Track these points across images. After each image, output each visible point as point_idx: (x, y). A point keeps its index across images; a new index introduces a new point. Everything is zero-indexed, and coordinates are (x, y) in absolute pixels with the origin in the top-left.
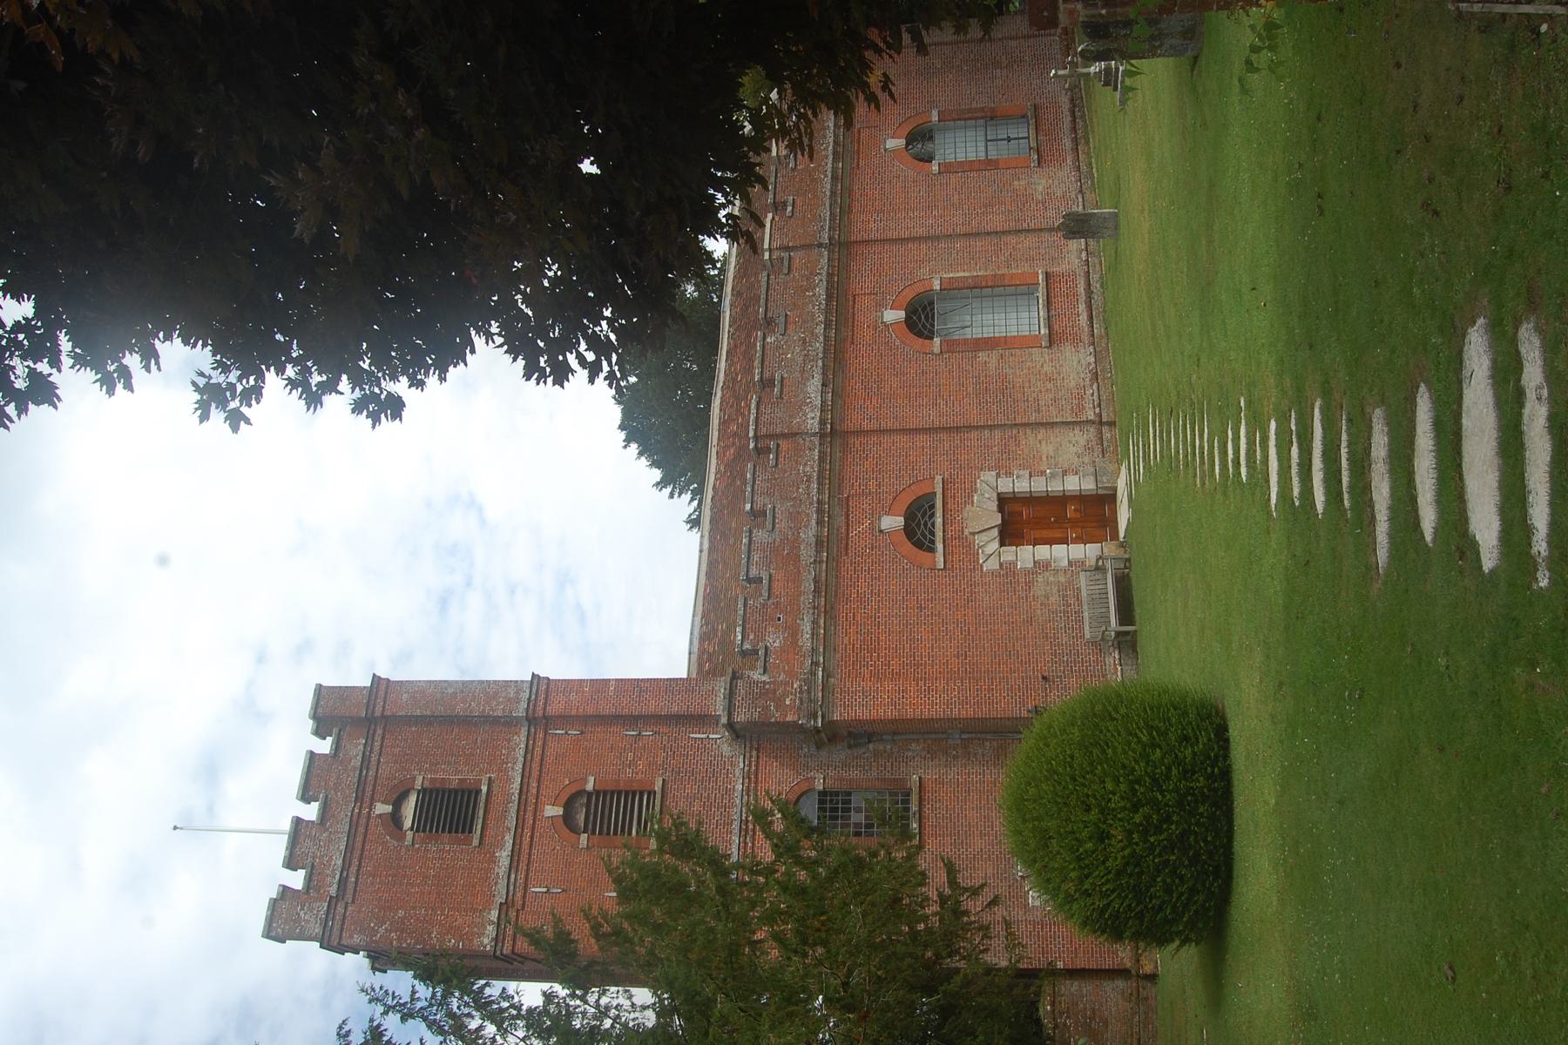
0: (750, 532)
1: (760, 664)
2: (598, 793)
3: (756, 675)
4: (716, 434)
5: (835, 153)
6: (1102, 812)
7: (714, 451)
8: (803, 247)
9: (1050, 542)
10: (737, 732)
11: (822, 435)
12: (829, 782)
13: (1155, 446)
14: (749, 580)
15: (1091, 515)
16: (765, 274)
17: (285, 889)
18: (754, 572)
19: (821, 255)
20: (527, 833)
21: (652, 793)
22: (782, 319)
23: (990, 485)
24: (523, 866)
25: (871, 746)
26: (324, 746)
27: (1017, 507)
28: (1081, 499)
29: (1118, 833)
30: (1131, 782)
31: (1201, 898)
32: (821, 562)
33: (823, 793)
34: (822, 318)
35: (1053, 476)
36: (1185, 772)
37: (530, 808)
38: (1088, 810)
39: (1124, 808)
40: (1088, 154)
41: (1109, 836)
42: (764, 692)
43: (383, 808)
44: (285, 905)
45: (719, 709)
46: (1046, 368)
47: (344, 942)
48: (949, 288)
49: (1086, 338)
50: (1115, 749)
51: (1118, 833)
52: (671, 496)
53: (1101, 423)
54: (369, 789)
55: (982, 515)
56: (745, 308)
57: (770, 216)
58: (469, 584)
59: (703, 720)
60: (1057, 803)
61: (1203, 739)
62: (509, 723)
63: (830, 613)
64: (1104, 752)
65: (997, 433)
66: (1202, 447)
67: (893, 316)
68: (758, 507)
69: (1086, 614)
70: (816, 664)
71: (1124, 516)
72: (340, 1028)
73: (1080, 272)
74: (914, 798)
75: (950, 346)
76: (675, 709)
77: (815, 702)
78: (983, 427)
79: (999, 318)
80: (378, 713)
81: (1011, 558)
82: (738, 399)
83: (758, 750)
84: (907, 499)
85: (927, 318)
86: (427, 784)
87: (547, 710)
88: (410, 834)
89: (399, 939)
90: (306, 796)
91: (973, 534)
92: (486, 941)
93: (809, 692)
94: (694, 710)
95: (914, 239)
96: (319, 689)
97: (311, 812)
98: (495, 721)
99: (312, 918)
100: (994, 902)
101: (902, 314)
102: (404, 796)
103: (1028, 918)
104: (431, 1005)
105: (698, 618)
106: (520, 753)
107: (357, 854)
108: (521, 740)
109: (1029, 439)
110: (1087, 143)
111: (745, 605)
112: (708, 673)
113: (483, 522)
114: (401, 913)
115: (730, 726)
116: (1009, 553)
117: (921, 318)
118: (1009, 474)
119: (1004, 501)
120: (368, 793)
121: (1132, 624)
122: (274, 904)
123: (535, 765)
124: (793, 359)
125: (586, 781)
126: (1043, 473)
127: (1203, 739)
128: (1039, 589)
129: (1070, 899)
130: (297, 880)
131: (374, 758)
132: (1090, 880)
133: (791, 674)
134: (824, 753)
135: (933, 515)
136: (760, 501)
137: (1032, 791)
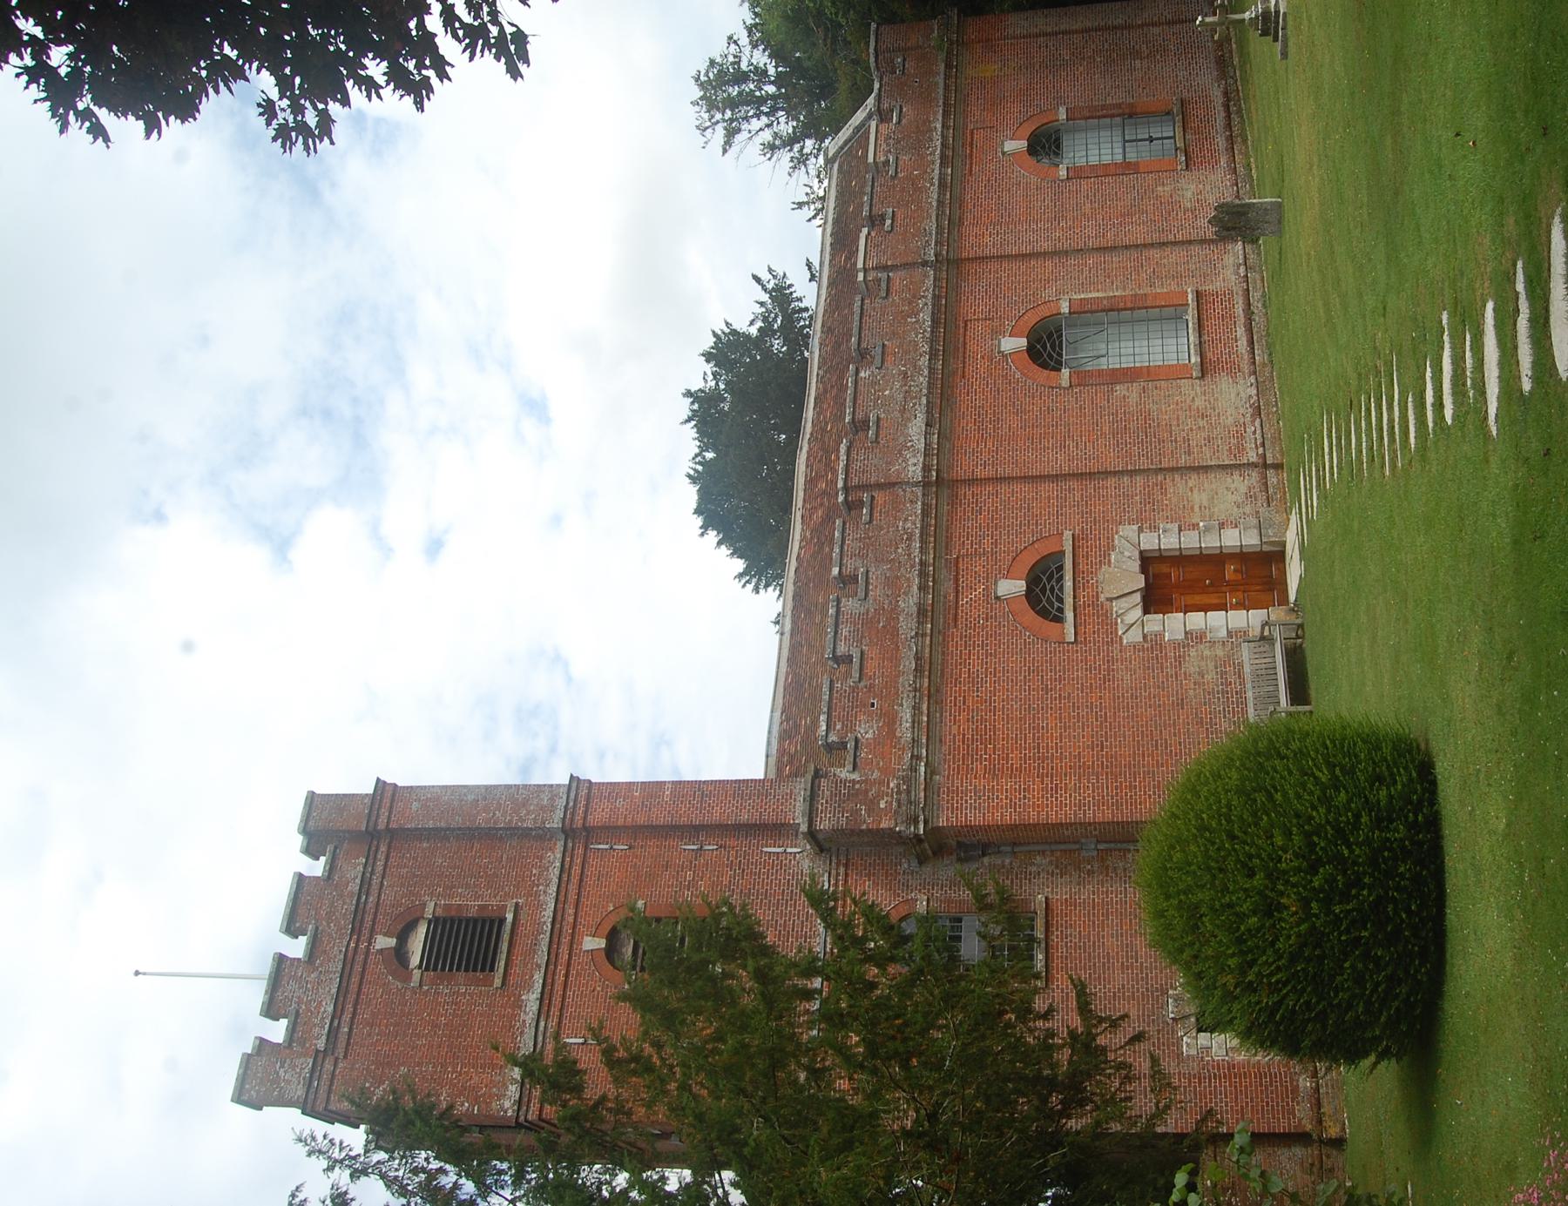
0: (838, 601)
3: (844, 773)
4: (801, 494)
5: (943, 156)
6: (1269, 876)
7: (799, 515)
8: (905, 266)
9: (1205, 609)
10: (820, 843)
11: (926, 484)
13: (1331, 459)
14: (836, 659)
15: (1256, 574)
16: (858, 298)
17: (262, 1043)
18: (842, 649)
19: (926, 276)
20: (561, 970)
22: (879, 350)
24: (555, 1011)
25: (986, 860)
26: (317, 868)
27: (1164, 569)
28: (1242, 557)
30: (1308, 835)
31: (1403, 990)
34: (926, 348)
35: (1207, 529)
36: (1379, 820)
37: (565, 940)
38: (1251, 875)
39: (1298, 870)
40: (1247, 156)
41: (1281, 908)
42: (854, 793)
43: (384, 942)
46: (1197, 403)
47: (332, 1107)
48: (1081, 311)
49: (1246, 368)
52: (756, 590)
53: (1265, 466)
54: (368, 918)
55: (1121, 576)
56: (838, 345)
57: (865, 231)
58: (553, 750)
59: (778, 830)
60: (1209, 869)
61: (1402, 779)
62: (542, 836)
63: (934, 696)
64: (1271, 798)
65: (1139, 479)
66: (1391, 421)
67: (1013, 344)
68: (848, 571)
69: (1250, 694)
70: (919, 758)
71: (1294, 572)
72: (293, 1196)
73: (1238, 290)
74: (1040, 923)
75: (1082, 378)
76: (744, 817)
77: (917, 803)
78: (1122, 473)
79: (1141, 346)
80: (381, 826)
82: (827, 452)
83: (846, 866)
84: (1030, 559)
86: (439, 912)
87: (588, 822)
88: (417, 974)
90: (292, 927)
91: (1111, 600)
92: (507, 1104)
93: (908, 792)
94: (769, 817)
96: (312, 799)
97: (297, 948)
98: (525, 834)
99: (294, 1077)
100: (1138, 1038)
102: (410, 927)
105: (778, 714)
106: (554, 874)
107: (351, 997)
109: (1179, 487)
110: (1245, 141)
111: (831, 690)
113: (569, 679)
115: (812, 835)
116: (1154, 622)
117: (1045, 347)
119: (1148, 561)
121: (1307, 703)
122: (247, 1060)
123: (573, 888)
124: (891, 397)
126: (1195, 526)
127: (1402, 779)
128: (1191, 666)
129: (1229, 997)
130: (277, 1031)
131: (376, 881)
132: (1256, 969)
133: (885, 771)
134: (927, 869)
135: (1061, 578)
137: (1177, 856)
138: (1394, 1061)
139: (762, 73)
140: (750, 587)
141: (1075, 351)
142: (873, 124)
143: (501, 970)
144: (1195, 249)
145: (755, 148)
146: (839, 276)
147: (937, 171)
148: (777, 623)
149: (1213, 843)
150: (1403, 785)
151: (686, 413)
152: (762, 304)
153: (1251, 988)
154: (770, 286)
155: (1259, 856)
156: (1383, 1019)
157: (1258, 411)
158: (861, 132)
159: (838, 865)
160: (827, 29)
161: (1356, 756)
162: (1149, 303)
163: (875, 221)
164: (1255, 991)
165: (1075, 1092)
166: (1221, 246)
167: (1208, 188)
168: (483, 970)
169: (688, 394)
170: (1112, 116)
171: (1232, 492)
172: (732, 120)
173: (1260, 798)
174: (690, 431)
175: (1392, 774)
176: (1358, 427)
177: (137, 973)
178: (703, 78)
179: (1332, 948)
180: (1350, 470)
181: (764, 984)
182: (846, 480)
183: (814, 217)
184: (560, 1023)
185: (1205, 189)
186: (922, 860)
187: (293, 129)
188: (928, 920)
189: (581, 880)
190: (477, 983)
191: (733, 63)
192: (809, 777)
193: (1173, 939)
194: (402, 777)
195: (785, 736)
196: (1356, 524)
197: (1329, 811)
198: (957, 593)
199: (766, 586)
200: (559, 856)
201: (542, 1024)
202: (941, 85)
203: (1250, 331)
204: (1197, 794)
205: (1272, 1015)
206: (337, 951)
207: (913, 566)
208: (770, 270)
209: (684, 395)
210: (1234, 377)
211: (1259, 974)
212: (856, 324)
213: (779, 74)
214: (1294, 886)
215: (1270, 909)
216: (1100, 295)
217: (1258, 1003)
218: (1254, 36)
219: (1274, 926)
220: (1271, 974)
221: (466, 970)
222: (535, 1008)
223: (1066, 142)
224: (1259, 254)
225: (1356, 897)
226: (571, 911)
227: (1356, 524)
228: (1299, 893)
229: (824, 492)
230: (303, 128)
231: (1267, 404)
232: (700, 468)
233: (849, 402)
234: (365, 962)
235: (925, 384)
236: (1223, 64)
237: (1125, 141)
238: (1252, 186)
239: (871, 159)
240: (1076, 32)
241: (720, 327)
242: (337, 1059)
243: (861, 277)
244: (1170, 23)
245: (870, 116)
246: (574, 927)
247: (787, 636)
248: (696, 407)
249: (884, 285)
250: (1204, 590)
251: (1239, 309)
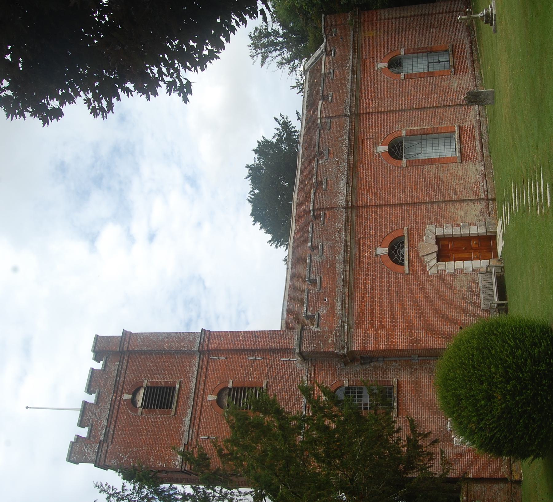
0: (311, 257)
1: (316, 322)
2: (234, 388)
3: (314, 328)
4: (295, 211)
5: (353, 70)
6: (489, 384)
7: (294, 219)
8: (337, 116)
9: (463, 260)
10: (304, 357)
11: (347, 208)
12: (351, 382)
13: (515, 202)
15: (484, 245)
16: (318, 130)
17: (78, 438)
18: (312, 277)
19: (346, 120)
20: (199, 408)
21: (261, 388)
22: (327, 152)
23: (431, 232)
24: (196, 425)
25: (372, 364)
26: (99, 366)
27: (446, 243)
28: (478, 238)
29: (498, 395)
30: (505, 368)
32: (346, 271)
33: (348, 388)
34: (346, 151)
37: (200, 396)
38: (482, 383)
39: (502, 382)
41: (494, 397)
42: (318, 337)
43: (127, 396)
44: (78, 445)
45: (295, 345)
47: (107, 464)
48: (411, 135)
49: (480, 158)
50: (496, 350)
51: (498, 395)
52: (276, 247)
53: (488, 199)
54: (120, 387)
55: (428, 246)
57: (321, 102)
59: (287, 351)
60: (465, 380)
61: (544, 344)
62: (190, 353)
63: (351, 296)
64: (490, 352)
65: (435, 206)
66: (540, 193)
67: (382, 149)
68: (315, 243)
69: (482, 296)
70: (344, 322)
73: (476, 125)
75: (411, 163)
76: (273, 346)
77: (344, 341)
78: (428, 203)
80: (125, 349)
81: (443, 268)
82: (306, 193)
83: (315, 366)
84: (390, 239)
85: (399, 150)
86: (149, 384)
87: (211, 348)
88: (140, 409)
89: (134, 462)
90: (89, 390)
91: (424, 256)
92: (177, 463)
93: (340, 336)
94: (283, 346)
95: (392, 111)
96: (97, 337)
98: (183, 352)
101: (386, 148)
102: (137, 390)
103: (455, 449)
104: (133, 493)
105: (286, 302)
106: (195, 369)
108: (196, 362)
109: (452, 209)
110: (479, 62)
111: (308, 293)
112: (291, 329)
114: (135, 449)
115: (301, 354)
116: (442, 265)
117: (396, 150)
118: (442, 226)
119: (439, 240)
120: (120, 389)
121: (506, 299)
122: (72, 444)
124: (332, 171)
125: (228, 382)
126: (458, 225)
127: (544, 344)
128: (457, 284)
129: (472, 433)
130: (84, 432)
131: (123, 372)
133: (331, 327)
134: (348, 368)
135: (403, 247)
136: (315, 241)
137: (451, 374)
138: (541, 458)
139: (276, 33)
140: (274, 246)
141: (408, 152)
142: (324, 57)
143: (174, 408)
144: (458, 108)
145: (274, 64)
146: (310, 120)
147: (350, 77)
148: (285, 260)
149: (466, 370)
150: (545, 347)
151: (247, 174)
152: (278, 129)
153: (482, 430)
154: (281, 122)
155: (485, 376)
156: (536, 443)
157: (485, 177)
158: (318, 60)
159: (311, 366)
160: (304, 14)
161: (525, 334)
162: (439, 131)
163: (325, 97)
164: (483, 430)
165: (410, 465)
166: (469, 107)
167: (463, 82)
168: (167, 408)
169: (248, 166)
170: (423, 52)
171: (474, 211)
172: (265, 53)
173: (486, 352)
174: (249, 182)
175: (540, 342)
176: (526, 192)
177: (27, 408)
178: (252, 35)
179: (515, 414)
180: (523, 208)
181: (283, 431)
182: (313, 206)
183: (300, 92)
184: (198, 430)
185: (462, 84)
186: (346, 364)
187: (98, 109)
188: (349, 390)
189: (206, 372)
191: (265, 29)
192: (299, 330)
193: (449, 408)
194: (134, 329)
195: (289, 311)
196: (525, 231)
197: (514, 358)
199: (280, 245)
200: (197, 361)
201: (191, 430)
202: (352, 40)
203: (481, 142)
204: (459, 350)
205: (491, 440)
206: (108, 400)
207: (341, 242)
208: (281, 115)
209: (246, 167)
210: (475, 162)
211: (485, 424)
212: (317, 141)
213: (284, 33)
214: (499, 388)
215: (489, 398)
216: (419, 128)
217: (485, 435)
218: (482, 23)
219: (491, 405)
220: (490, 424)
222: (188, 424)
223: (404, 63)
224: (485, 110)
225: (525, 393)
226: (203, 384)
227: (525, 231)
228: (501, 392)
229: (304, 210)
230: (101, 109)
231: (489, 174)
232: (253, 197)
233: (314, 173)
234: (119, 405)
235: (346, 166)
236: (469, 29)
237: (428, 63)
238: (482, 82)
239: (323, 72)
240: (408, 17)
241: (261, 139)
242: (108, 444)
243: (319, 121)
244: (447, 12)
245: (322, 53)
246: (204, 391)
247: (290, 270)
248: (251, 172)
249: (329, 125)
250: (463, 252)
251: (477, 134)
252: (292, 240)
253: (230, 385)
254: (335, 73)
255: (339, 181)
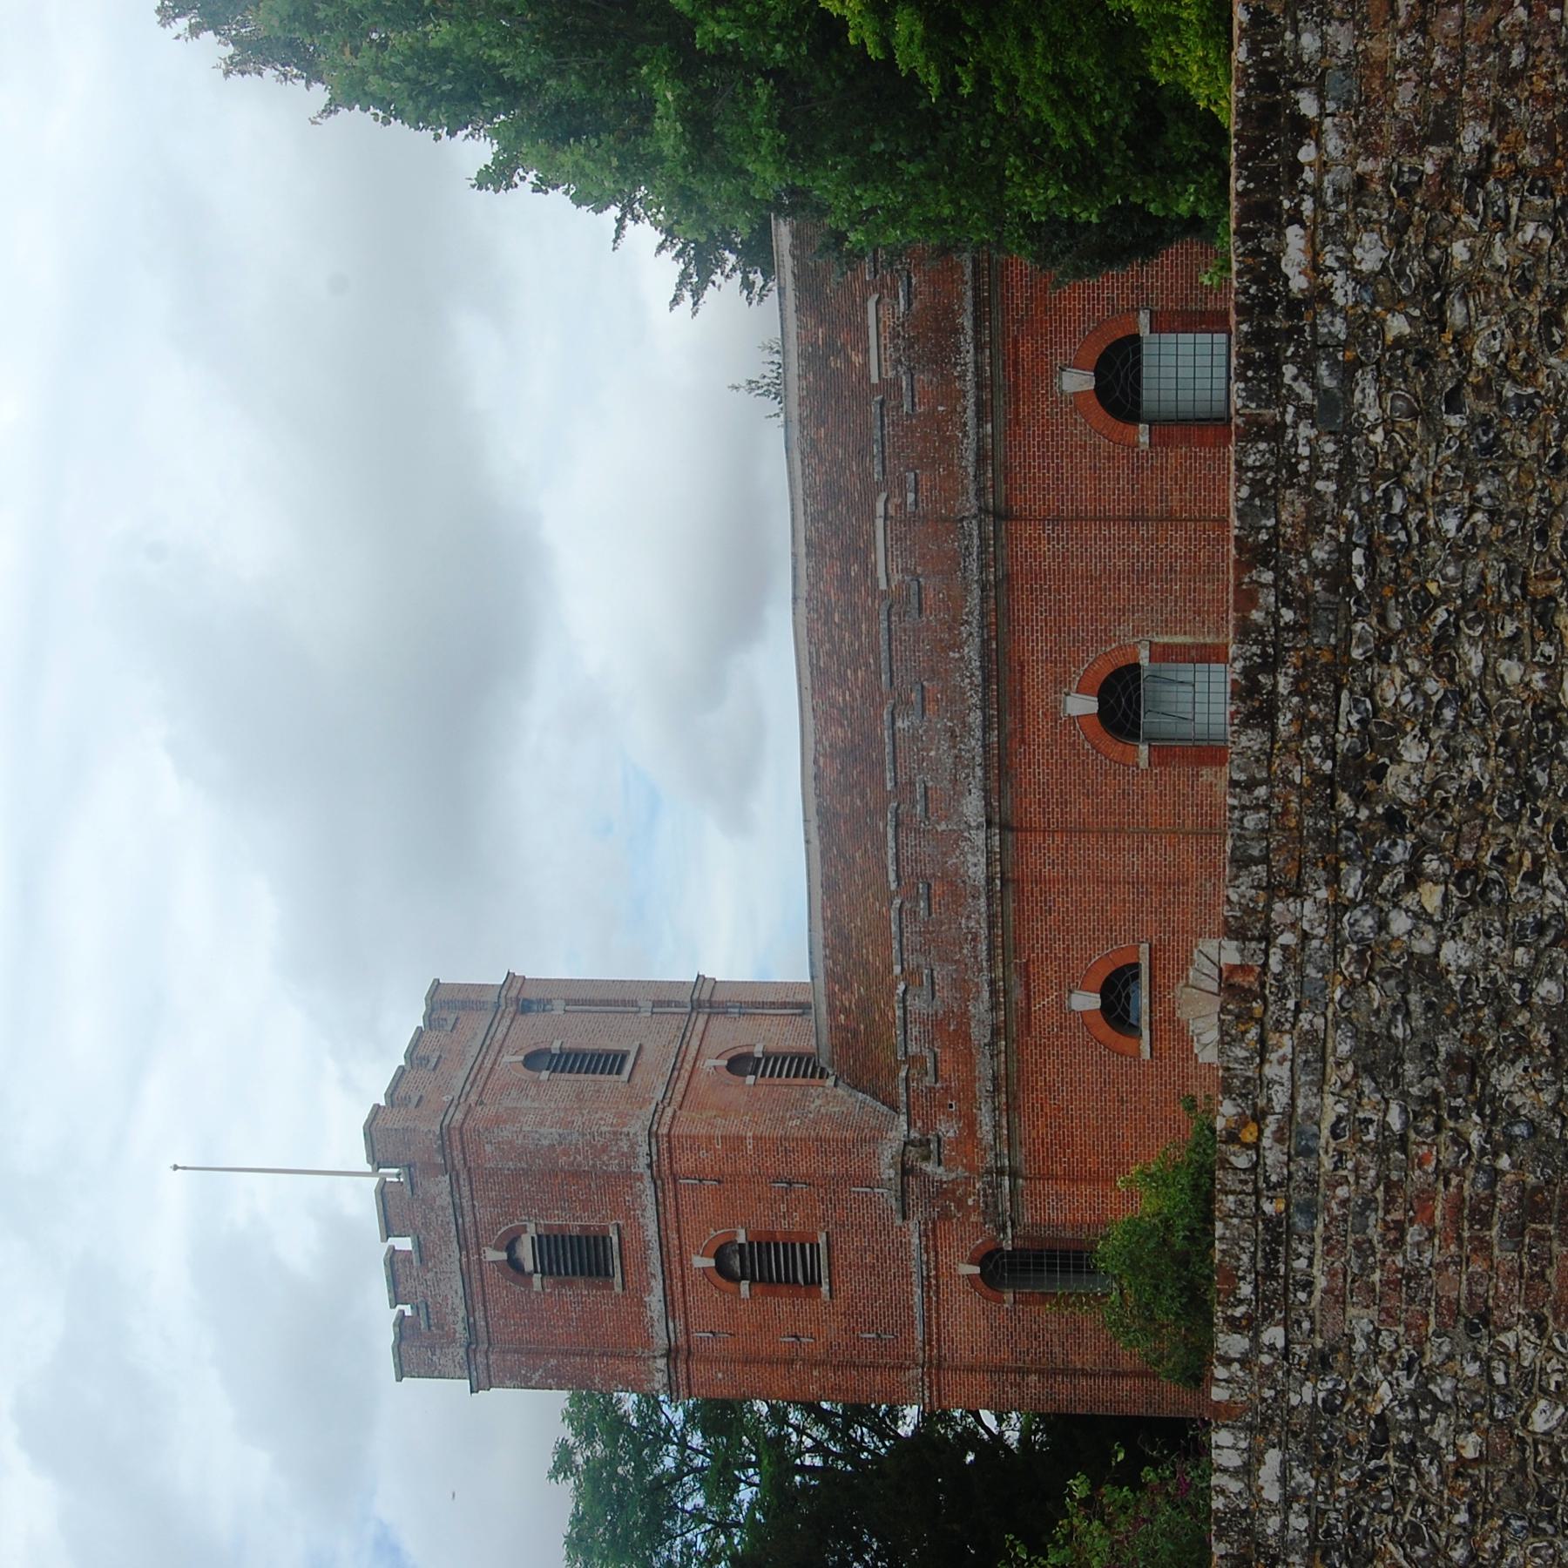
1: (934, 1157)
34: (975, 700)
57: (884, 496)
67: (1082, 705)
75: (1165, 753)
85: (1129, 701)
111: (907, 1089)
117: (1122, 702)
120: (472, 1240)
136: (912, 960)
177: (176, 1168)
190: (598, 1288)
198: (1028, 997)
201: (671, 1325)
207: (980, 970)
216: (1188, 640)
221: (582, 1274)
226: (675, 1236)
252: (788, 262)
253: (741, 1239)
254: (917, 386)
255: (962, 794)
